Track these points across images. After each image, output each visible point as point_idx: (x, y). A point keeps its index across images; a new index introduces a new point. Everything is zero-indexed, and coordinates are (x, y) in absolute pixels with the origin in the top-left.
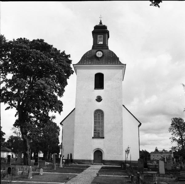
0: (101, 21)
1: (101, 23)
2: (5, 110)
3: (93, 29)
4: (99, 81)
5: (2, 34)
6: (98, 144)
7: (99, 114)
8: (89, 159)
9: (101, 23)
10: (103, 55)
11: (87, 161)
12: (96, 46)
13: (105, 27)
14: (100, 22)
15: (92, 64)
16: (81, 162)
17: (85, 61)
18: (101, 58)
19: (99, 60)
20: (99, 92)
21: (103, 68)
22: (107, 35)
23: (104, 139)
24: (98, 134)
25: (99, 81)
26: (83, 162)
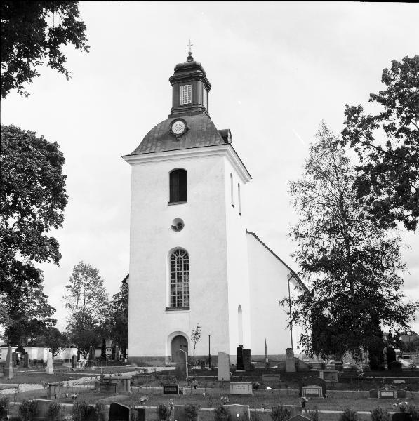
0: (190, 53)
1: (190, 58)
2: (240, 306)
3: (172, 73)
4: (178, 186)
5: (6, 123)
6: (181, 322)
7: (180, 261)
8: (159, 356)
9: (190, 58)
10: (187, 129)
11: (156, 359)
12: (179, 111)
13: (197, 67)
14: (188, 55)
15: (163, 150)
16: (144, 361)
17: (150, 145)
18: (182, 135)
19: (178, 141)
20: (179, 210)
21: (190, 156)
22: (200, 83)
23: (188, 311)
24: (179, 301)
25: (178, 186)
26: (147, 362)
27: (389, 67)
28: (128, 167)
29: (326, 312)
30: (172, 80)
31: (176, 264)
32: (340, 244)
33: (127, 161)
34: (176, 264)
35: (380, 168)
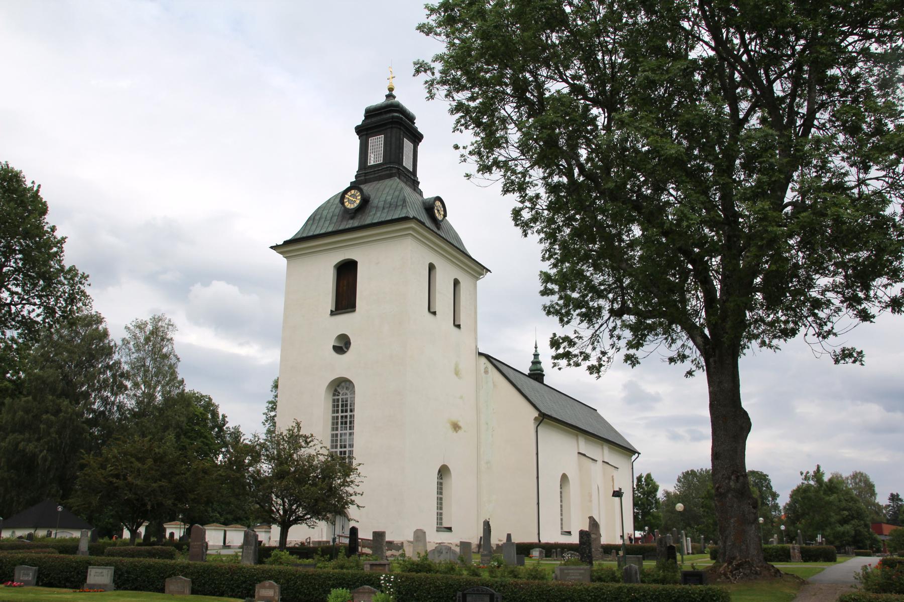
1: (390, 96)
7: (341, 387)
13: (398, 108)
14: (387, 92)
20: (345, 323)
27: (644, 475)
28: (280, 260)
29: (676, 297)
30: (359, 130)
31: (340, 420)
32: (689, 227)
33: (281, 253)
34: (340, 420)
35: (782, 46)
